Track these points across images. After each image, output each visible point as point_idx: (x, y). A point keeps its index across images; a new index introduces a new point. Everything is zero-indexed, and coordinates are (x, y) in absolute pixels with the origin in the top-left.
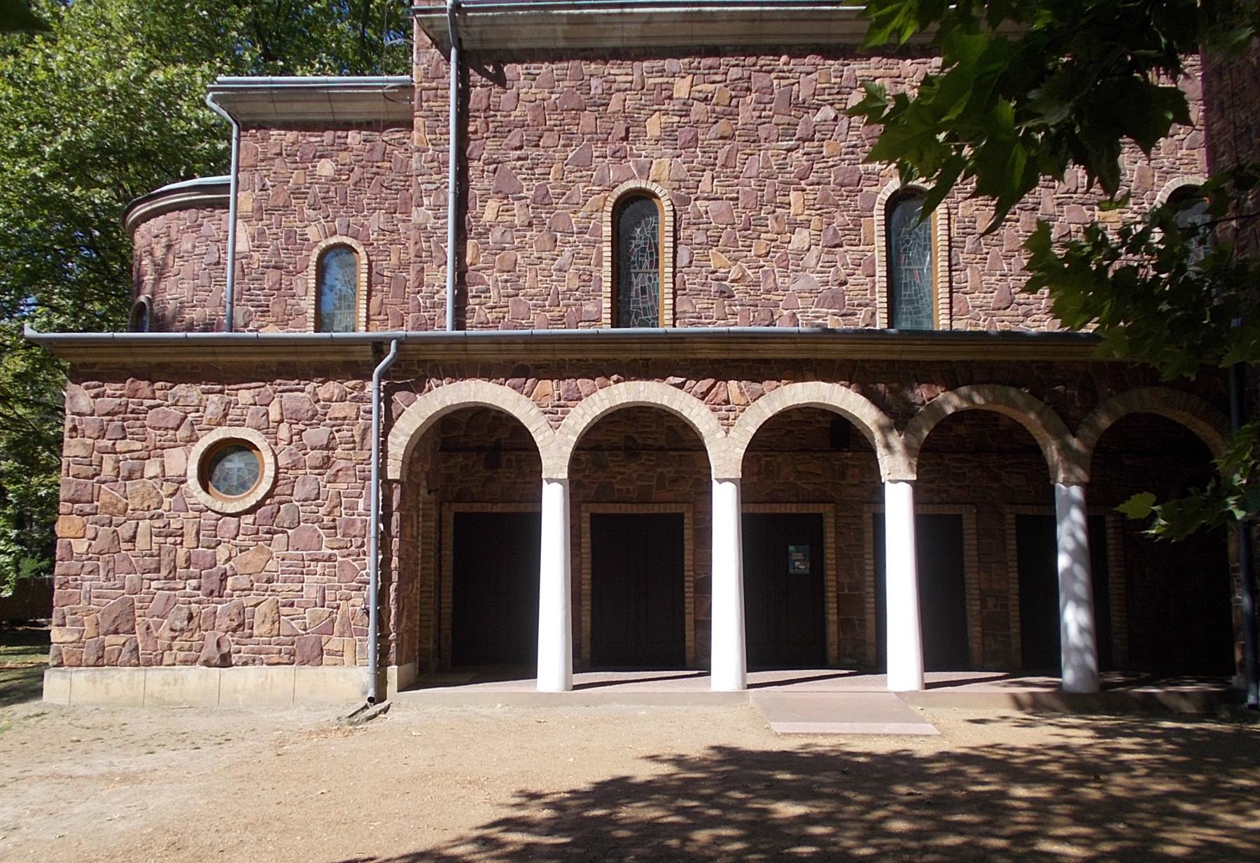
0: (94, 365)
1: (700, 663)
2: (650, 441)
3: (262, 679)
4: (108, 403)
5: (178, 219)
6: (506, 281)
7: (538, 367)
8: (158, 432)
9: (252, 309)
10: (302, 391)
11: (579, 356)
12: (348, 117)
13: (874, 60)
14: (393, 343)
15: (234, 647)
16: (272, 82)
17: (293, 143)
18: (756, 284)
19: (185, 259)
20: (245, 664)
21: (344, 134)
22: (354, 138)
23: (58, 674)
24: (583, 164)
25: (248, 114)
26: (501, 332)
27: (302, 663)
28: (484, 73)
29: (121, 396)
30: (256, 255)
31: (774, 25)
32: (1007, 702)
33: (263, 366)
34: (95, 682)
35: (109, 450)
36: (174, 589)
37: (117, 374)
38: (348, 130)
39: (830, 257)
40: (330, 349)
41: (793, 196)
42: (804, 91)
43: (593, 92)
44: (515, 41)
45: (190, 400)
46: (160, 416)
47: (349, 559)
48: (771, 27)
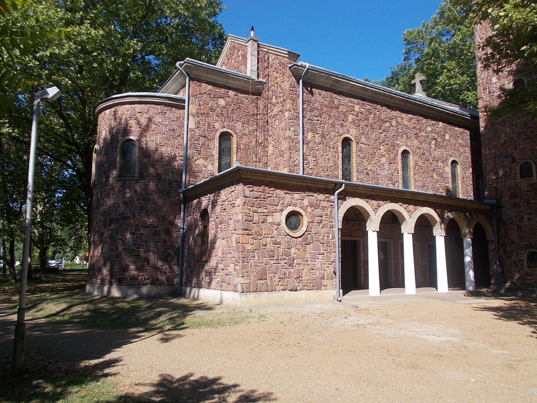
0: (250, 179)
1: (365, 286)
2: (351, 218)
3: (307, 295)
4: (257, 194)
5: (154, 108)
6: (315, 161)
7: (372, 196)
8: (271, 206)
9: (195, 152)
10: (313, 196)
11: (381, 194)
12: (230, 85)
13: (397, 111)
14: (344, 185)
15: (297, 284)
16: (207, 66)
17: (210, 90)
18: (374, 172)
19: (158, 125)
20: (301, 290)
21: (228, 91)
22: (231, 93)
23: (244, 295)
24: (333, 125)
25: (195, 75)
26: (313, 177)
27: (317, 289)
28: (307, 90)
29: (260, 192)
30: (197, 130)
31: (379, 96)
32: (463, 295)
33: (302, 186)
34: (256, 298)
35: (256, 211)
36: (279, 264)
37: (258, 184)
38: (229, 90)
39: (390, 167)
40: (323, 183)
41: (382, 147)
42: (383, 117)
43: (335, 103)
44: (316, 81)
45: (281, 195)
46: (272, 200)
47: (328, 254)
48: (378, 96)
